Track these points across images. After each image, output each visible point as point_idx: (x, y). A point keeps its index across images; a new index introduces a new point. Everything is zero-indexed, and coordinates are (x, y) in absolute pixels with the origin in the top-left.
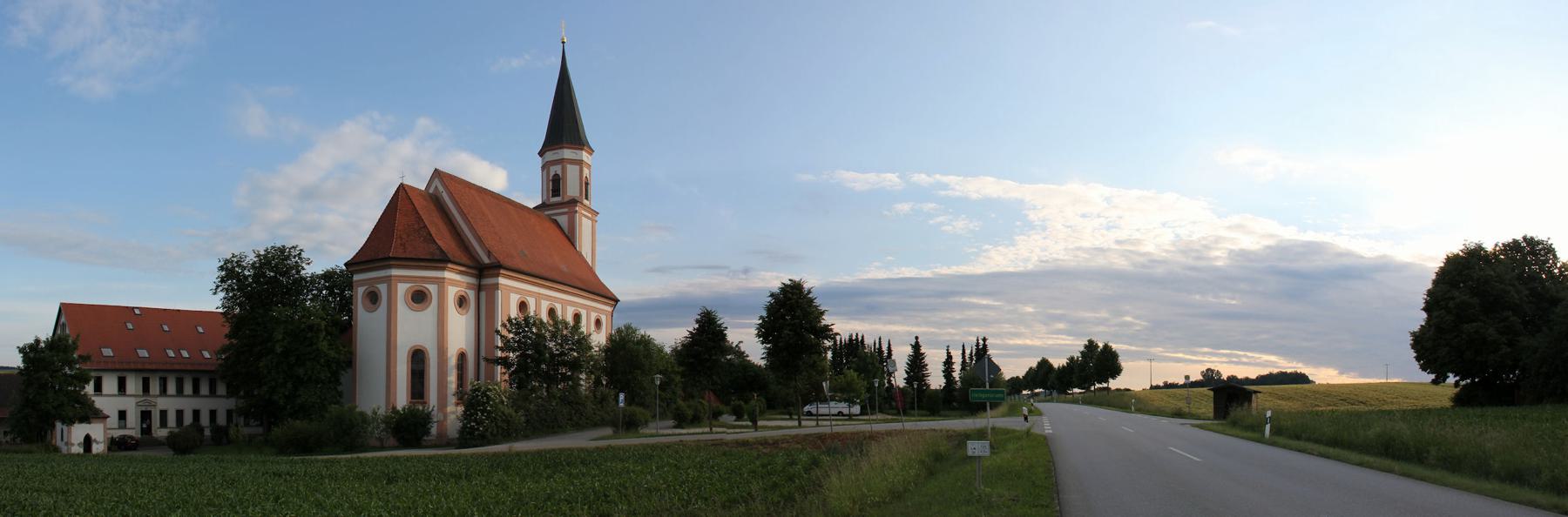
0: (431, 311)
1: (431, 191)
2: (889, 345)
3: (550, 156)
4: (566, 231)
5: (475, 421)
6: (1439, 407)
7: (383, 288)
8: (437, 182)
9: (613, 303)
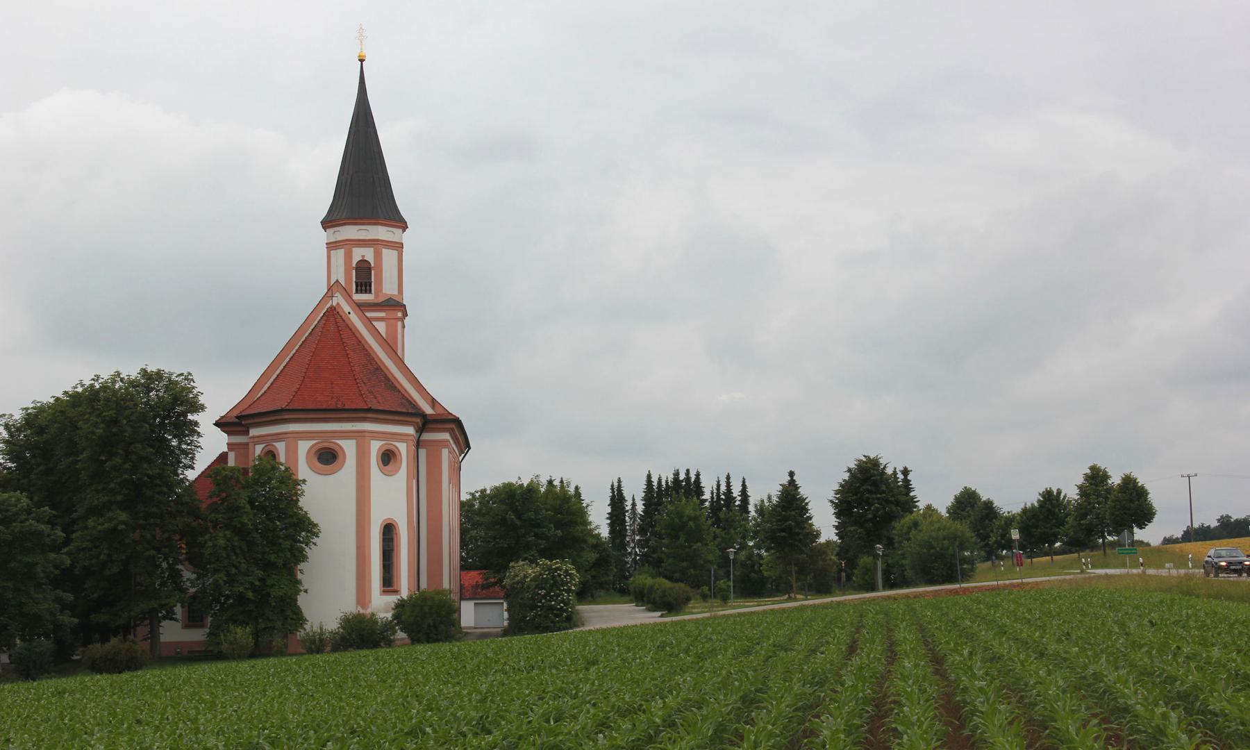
2: (744, 486)
5: (563, 601)
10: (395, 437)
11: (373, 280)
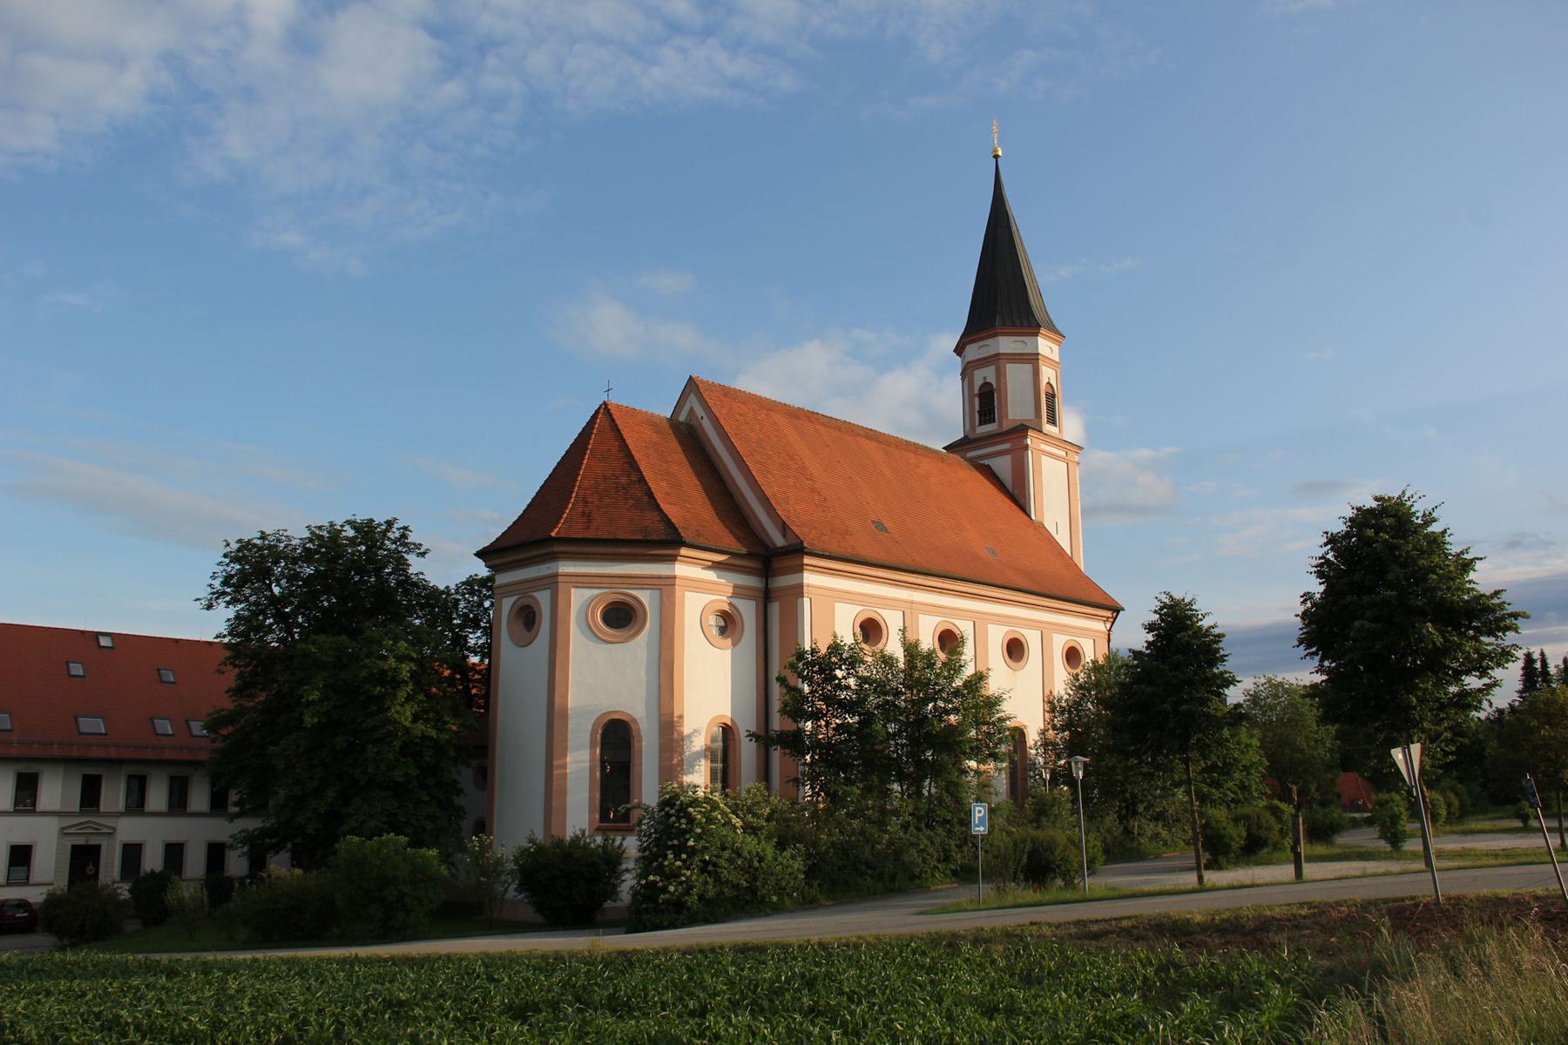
0: (640, 645)
1: (682, 418)
3: (973, 352)
4: (1010, 488)
6: (1501, 896)
7: (543, 598)
8: (693, 401)
9: (1109, 614)
11: (996, 405)
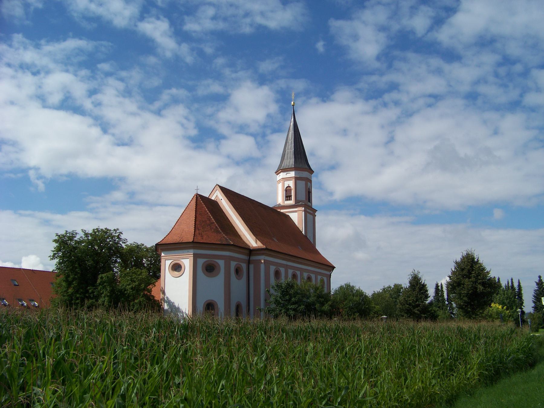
10: (300, 260)
